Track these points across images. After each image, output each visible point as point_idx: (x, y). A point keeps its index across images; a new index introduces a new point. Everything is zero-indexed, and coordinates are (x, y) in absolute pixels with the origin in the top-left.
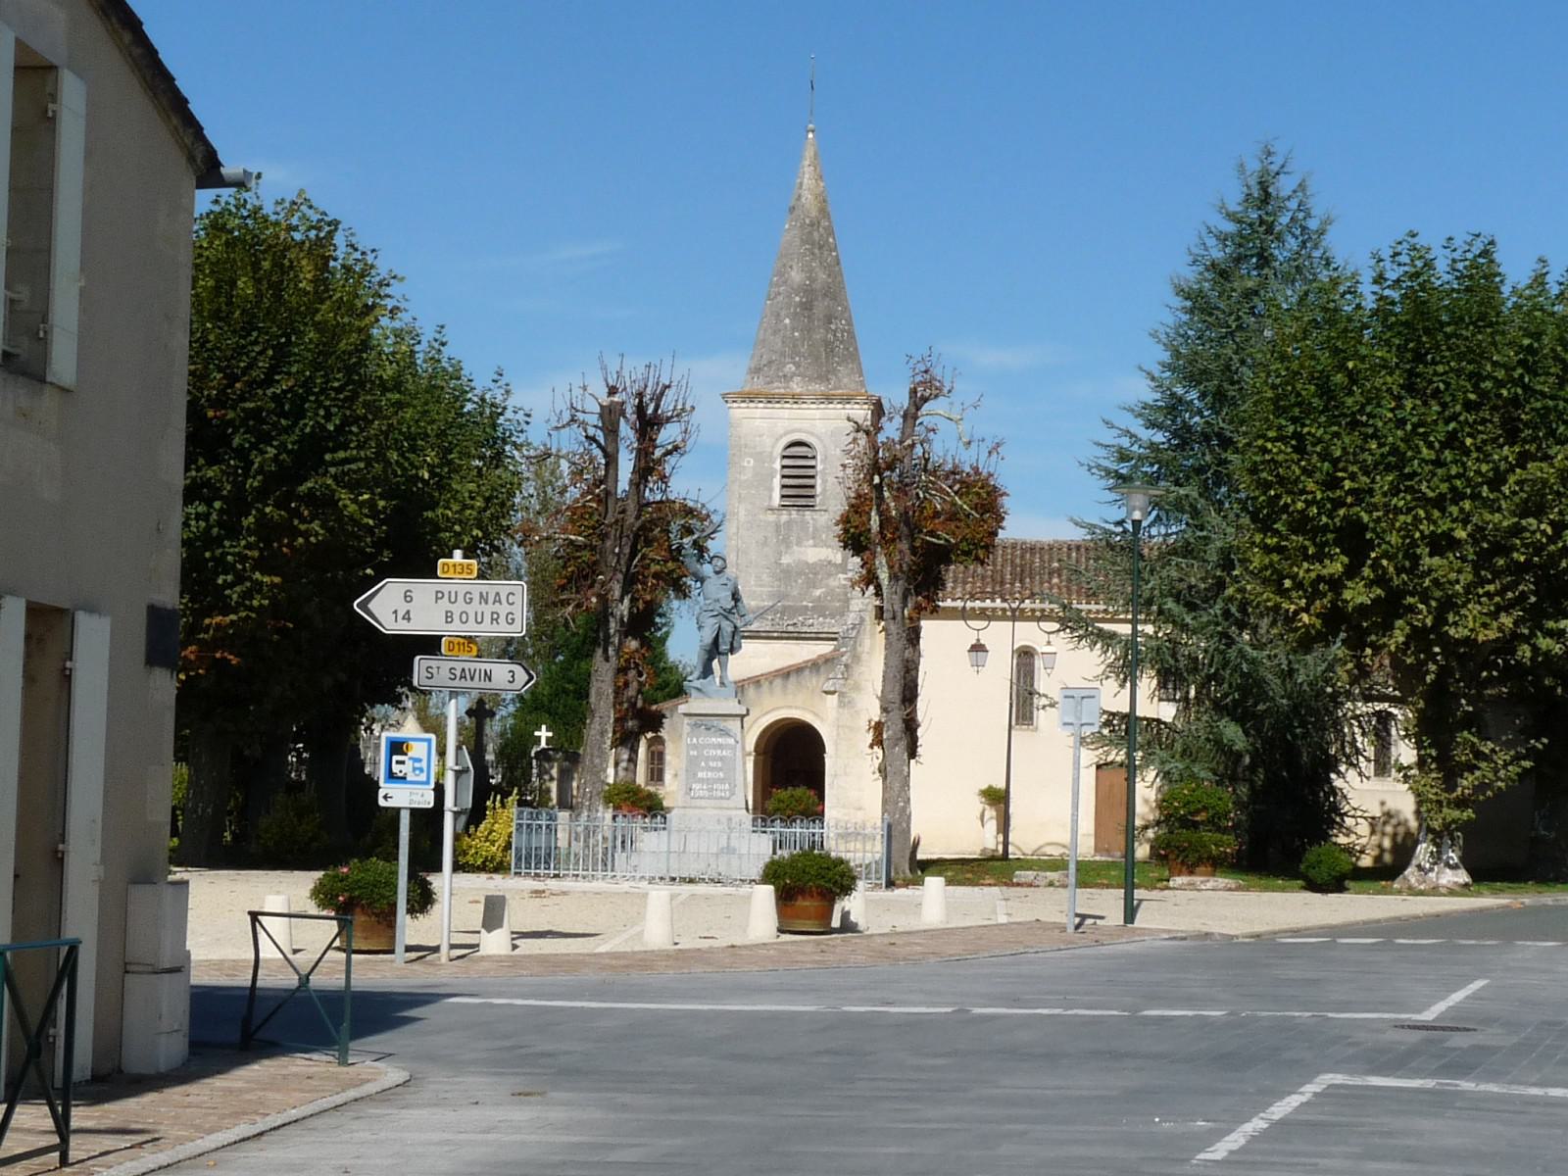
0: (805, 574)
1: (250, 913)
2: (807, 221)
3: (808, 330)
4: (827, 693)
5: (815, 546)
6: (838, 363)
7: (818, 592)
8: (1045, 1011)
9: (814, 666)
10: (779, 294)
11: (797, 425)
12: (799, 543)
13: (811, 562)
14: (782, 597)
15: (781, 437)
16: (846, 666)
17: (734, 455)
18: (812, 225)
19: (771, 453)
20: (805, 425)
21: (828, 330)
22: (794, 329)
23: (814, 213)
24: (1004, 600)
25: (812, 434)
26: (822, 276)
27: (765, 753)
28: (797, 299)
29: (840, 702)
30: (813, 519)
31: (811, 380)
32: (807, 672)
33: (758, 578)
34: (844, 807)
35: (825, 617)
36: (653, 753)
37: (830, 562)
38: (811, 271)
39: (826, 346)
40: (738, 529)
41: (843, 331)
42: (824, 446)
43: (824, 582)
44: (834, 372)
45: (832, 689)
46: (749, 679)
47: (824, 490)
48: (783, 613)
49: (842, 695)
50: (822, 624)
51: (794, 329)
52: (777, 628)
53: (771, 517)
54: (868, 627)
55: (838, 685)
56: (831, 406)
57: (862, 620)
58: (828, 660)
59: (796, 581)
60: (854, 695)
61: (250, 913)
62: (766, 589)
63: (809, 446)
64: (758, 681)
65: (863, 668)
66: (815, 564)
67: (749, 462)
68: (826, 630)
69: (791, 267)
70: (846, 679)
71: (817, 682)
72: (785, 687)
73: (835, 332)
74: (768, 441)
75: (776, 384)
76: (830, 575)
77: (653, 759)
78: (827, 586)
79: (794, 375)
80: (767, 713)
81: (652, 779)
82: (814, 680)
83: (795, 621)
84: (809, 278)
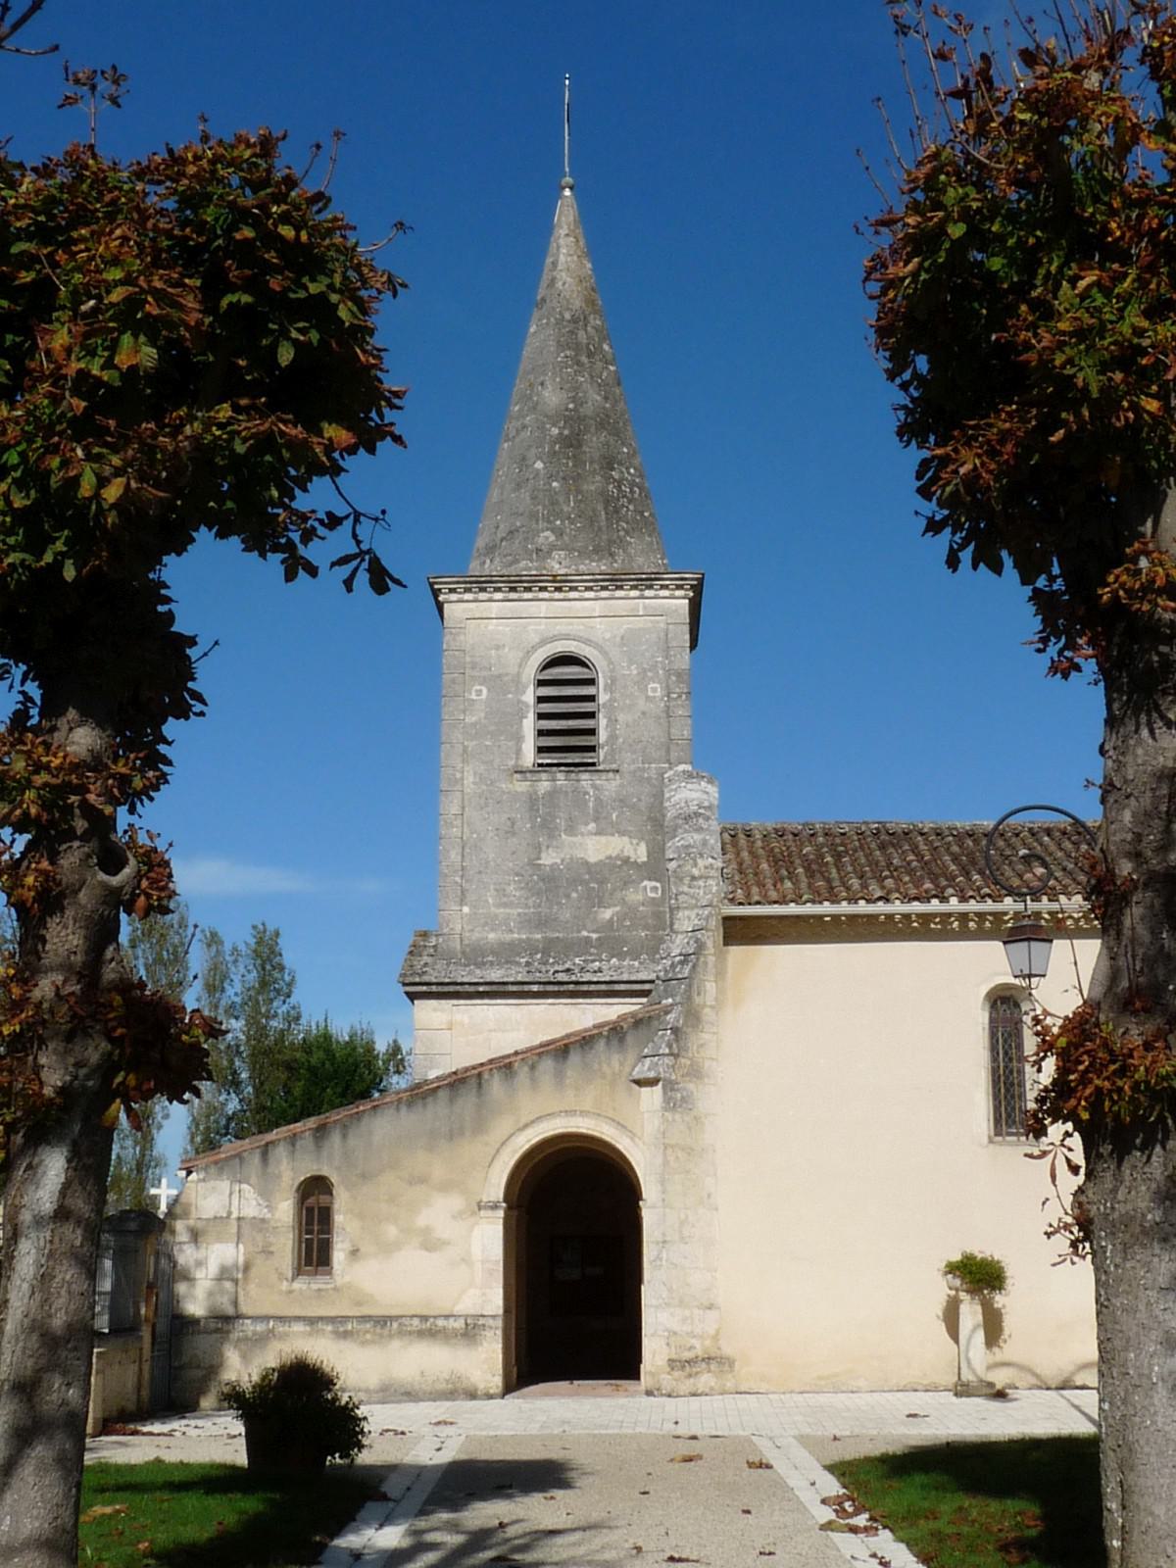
0: (583, 882)
1: (1049, 1238)
2: (567, 316)
3: (572, 482)
4: (639, 1083)
5: (599, 833)
6: (627, 532)
7: (607, 914)
8: (315, 1254)
9: (615, 1033)
10: (524, 427)
11: (562, 627)
12: (571, 830)
13: (592, 860)
14: (542, 923)
15: (534, 648)
16: (675, 1030)
17: (453, 681)
18: (574, 320)
19: (519, 674)
20: (576, 627)
21: (608, 479)
22: (551, 477)
23: (578, 304)
24: (963, 899)
25: (587, 642)
26: (595, 397)
27: (519, 1207)
28: (555, 431)
29: (667, 1099)
30: (594, 787)
31: (583, 554)
32: (601, 1045)
33: (501, 892)
34: (682, 1303)
35: (621, 956)
36: (310, 1210)
37: (626, 861)
38: (576, 388)
39: (607, 503)
40: (463, 808)
41: (632, 484)
42: (610, 662)
43: (618, 895)
44: (622, 543)
45: (652, 1074)
46: (491, 1061)
47: (612, 737)
48: (546, 952)
49: (670, 1086)
50: (617, 968)
51: (551, 477)
52: (538, 977)
53: (521, 786)
54: (711, 959)
55: (662, 1067)
56: (620, 593)
57: (701, 946)
58: (638, 1022)
59: (568, 896)
60: (691, 1086)
61: (1049, 1238)
62: (515, 912)
63: (587, 667)
64: (509, 1066)
65: (705, 1036)
66: (600, 863)
67: (479, 693)
68: (625, 977)
69: (542, 384)
70: (676, 1056)
71: (621, 1064)
72: (559, 1076)
73: (619, 483)
74: (512, 657)
75: (523, 564)
76: (626, 884)
77: (310, 1222)
78: (623, 902)
79: (553, 548)
80: (526, 1126)
81: (309, 1262)
82: (616, 1059)
83: (567, 966)
84: (574, 400)
